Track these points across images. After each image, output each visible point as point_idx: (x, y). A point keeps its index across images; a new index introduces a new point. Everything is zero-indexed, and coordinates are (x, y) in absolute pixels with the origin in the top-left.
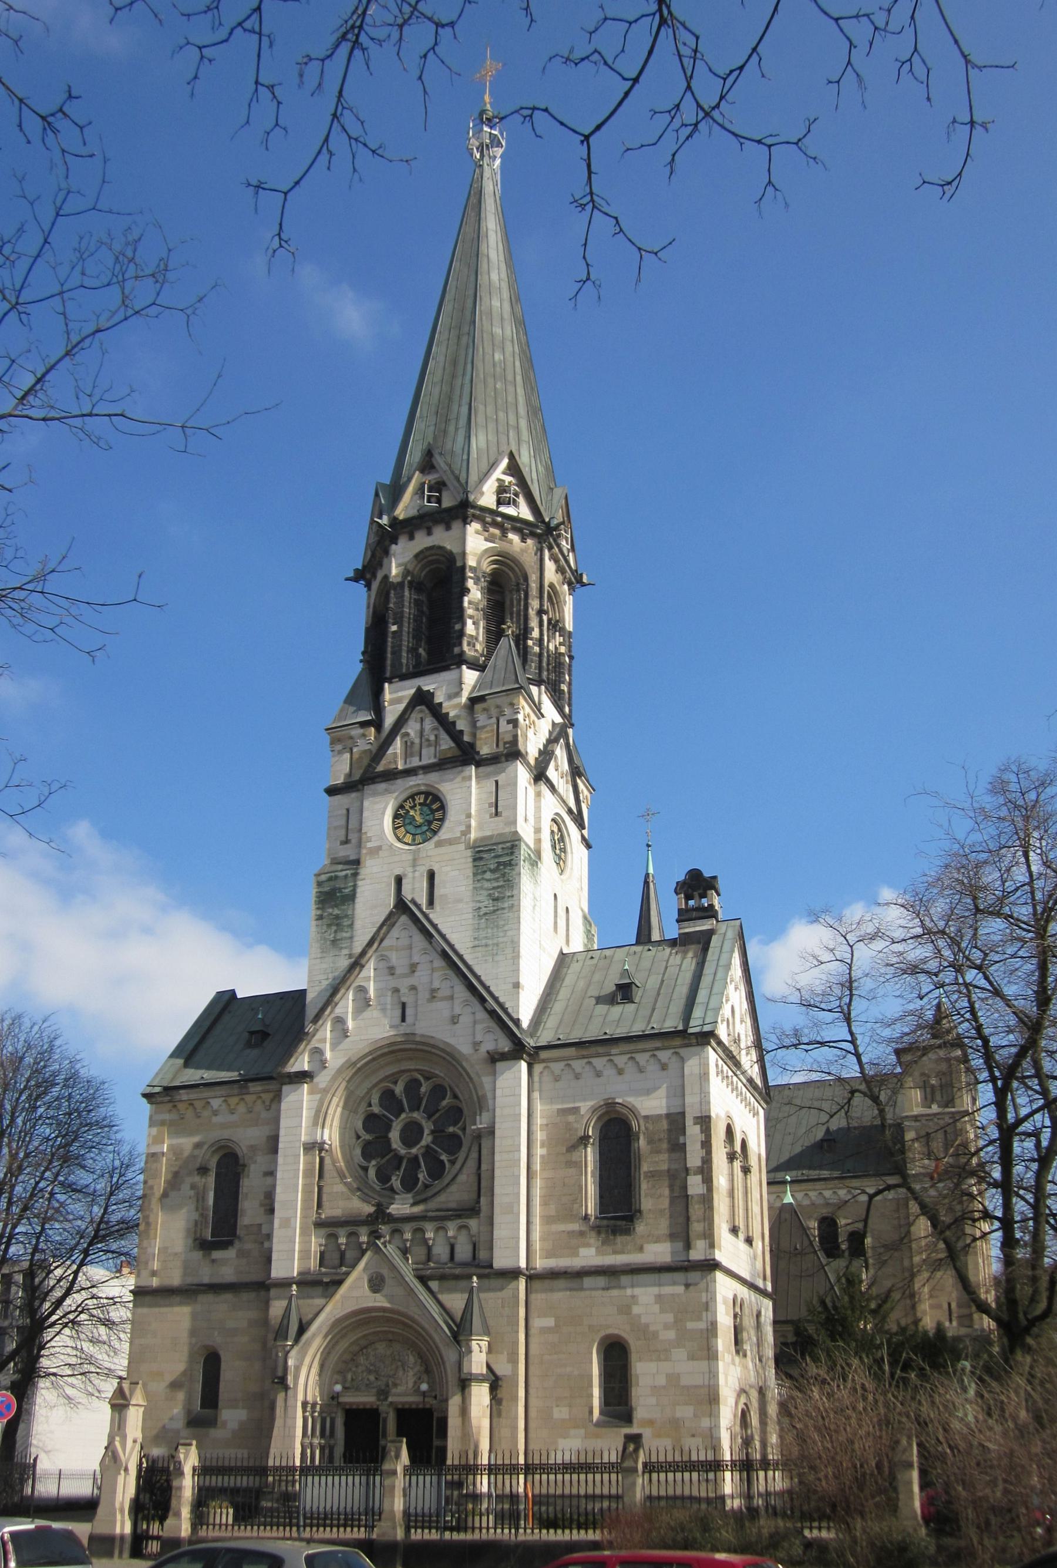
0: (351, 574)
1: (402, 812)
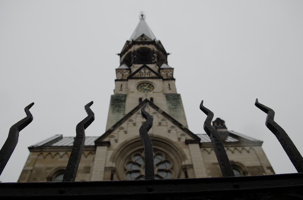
0: (117, 53)
1: (140, 86)
